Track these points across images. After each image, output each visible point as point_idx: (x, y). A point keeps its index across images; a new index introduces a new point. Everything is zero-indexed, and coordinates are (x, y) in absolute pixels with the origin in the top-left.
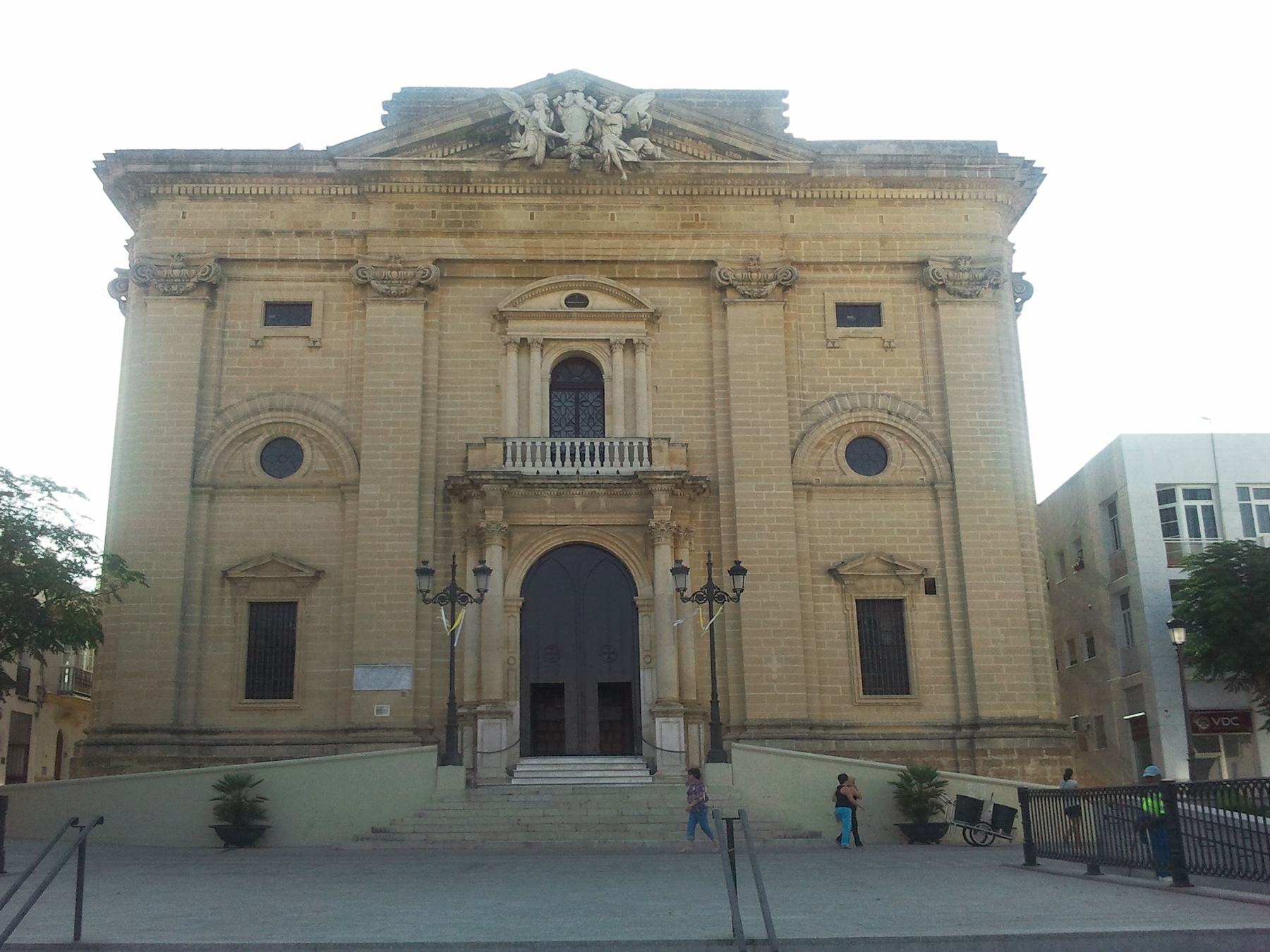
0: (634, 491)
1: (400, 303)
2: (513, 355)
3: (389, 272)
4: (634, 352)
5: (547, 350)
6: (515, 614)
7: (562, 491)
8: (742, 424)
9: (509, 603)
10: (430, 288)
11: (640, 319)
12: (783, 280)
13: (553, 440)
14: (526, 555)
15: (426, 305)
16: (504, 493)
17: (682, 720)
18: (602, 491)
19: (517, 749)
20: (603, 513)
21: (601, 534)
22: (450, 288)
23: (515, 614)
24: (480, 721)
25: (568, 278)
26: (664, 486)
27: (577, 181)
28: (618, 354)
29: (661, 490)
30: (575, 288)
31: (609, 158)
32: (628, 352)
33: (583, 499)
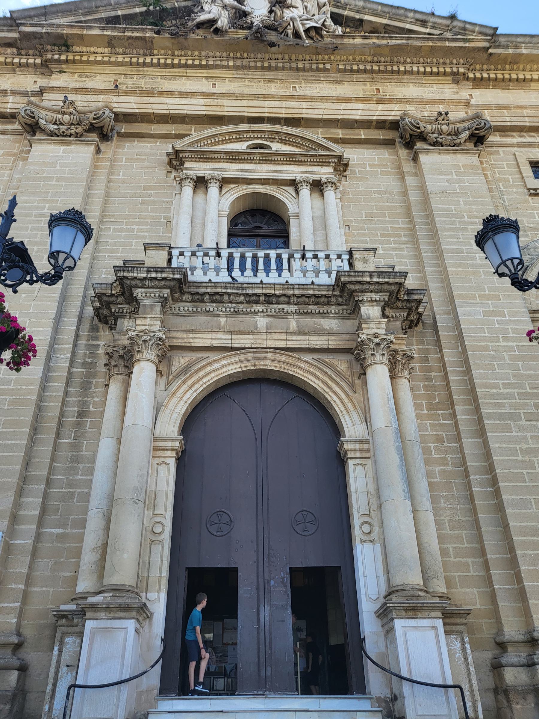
0: (334, 309)
1: (69, 143)
2: (188, 190)
3: (61, 116)
4: (322, 193)
5: (226, 191)
6: (168, 460)
7: (241, 306)
8: (454, 251)
9: (161, 444)
10: (105, 137)
11: (326, 164)
12: (476, 129)
13: (230, 251)
14: (189, 382)
15: (98, 151)
16: (164, 301)
17: (439, 623)
18: (292, 308)
19: (156, 674)
20: (294, 333)
21: (290, 360)
22: (127, 144)
23: (168, 460)
24: (89, 624)
25: (250, 127)
26: (376, 297)
27: (259, 56)
28: (305, 192)
29: (372, 301)
30: (258, 138)
31: (291, 24)
32: (316, 195)
33: (269, 319)
